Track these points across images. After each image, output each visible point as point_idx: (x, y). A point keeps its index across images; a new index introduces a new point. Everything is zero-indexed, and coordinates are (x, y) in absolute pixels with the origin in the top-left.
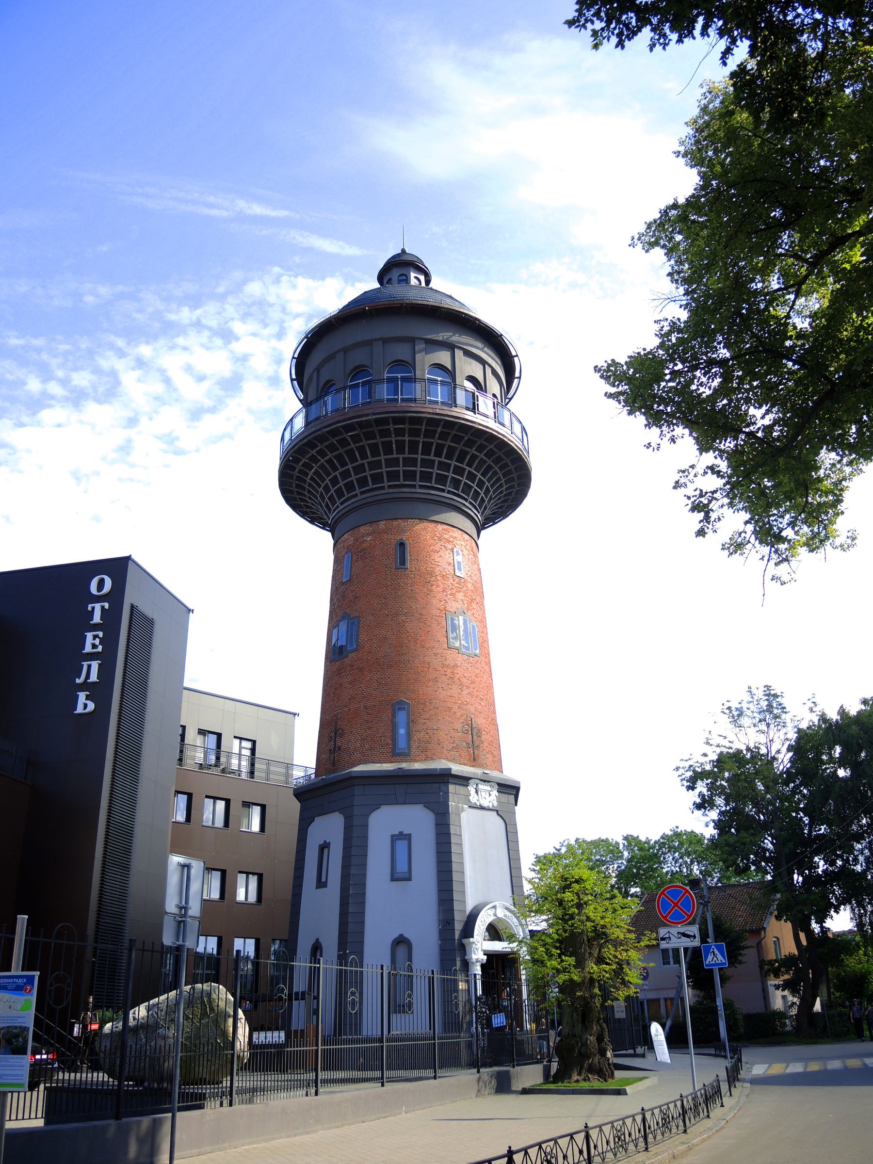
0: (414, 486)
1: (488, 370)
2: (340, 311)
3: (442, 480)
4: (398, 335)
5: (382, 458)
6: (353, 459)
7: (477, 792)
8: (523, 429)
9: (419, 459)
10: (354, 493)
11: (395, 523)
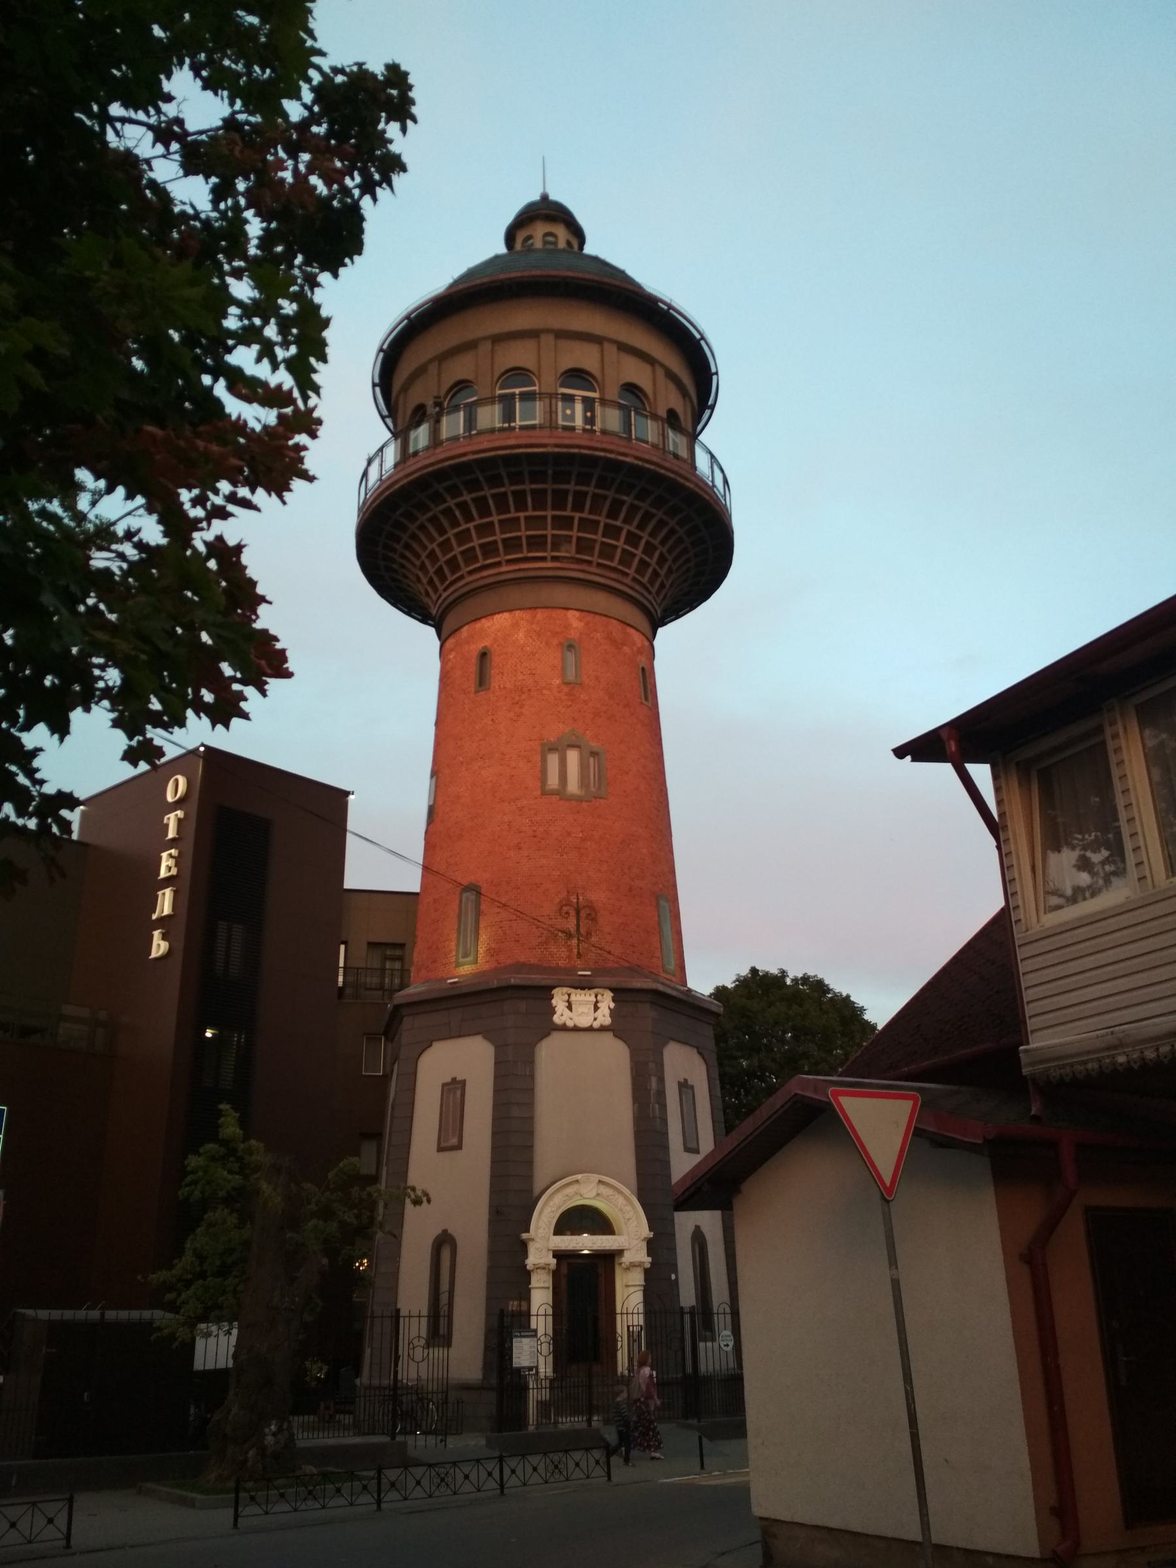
0: (499, 564)
1: (660, 373)
2: (451, 286)
3: (469, 555)
4: (519, 327)
5: (495, 518)
6: (612, 514)
7: (570, 1007)
8: (726, 481)
9: (496, 523)
10: (460, 573)
11: (478, 625)
